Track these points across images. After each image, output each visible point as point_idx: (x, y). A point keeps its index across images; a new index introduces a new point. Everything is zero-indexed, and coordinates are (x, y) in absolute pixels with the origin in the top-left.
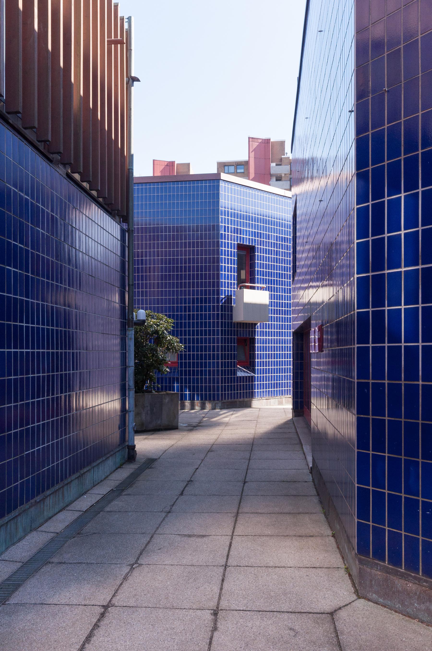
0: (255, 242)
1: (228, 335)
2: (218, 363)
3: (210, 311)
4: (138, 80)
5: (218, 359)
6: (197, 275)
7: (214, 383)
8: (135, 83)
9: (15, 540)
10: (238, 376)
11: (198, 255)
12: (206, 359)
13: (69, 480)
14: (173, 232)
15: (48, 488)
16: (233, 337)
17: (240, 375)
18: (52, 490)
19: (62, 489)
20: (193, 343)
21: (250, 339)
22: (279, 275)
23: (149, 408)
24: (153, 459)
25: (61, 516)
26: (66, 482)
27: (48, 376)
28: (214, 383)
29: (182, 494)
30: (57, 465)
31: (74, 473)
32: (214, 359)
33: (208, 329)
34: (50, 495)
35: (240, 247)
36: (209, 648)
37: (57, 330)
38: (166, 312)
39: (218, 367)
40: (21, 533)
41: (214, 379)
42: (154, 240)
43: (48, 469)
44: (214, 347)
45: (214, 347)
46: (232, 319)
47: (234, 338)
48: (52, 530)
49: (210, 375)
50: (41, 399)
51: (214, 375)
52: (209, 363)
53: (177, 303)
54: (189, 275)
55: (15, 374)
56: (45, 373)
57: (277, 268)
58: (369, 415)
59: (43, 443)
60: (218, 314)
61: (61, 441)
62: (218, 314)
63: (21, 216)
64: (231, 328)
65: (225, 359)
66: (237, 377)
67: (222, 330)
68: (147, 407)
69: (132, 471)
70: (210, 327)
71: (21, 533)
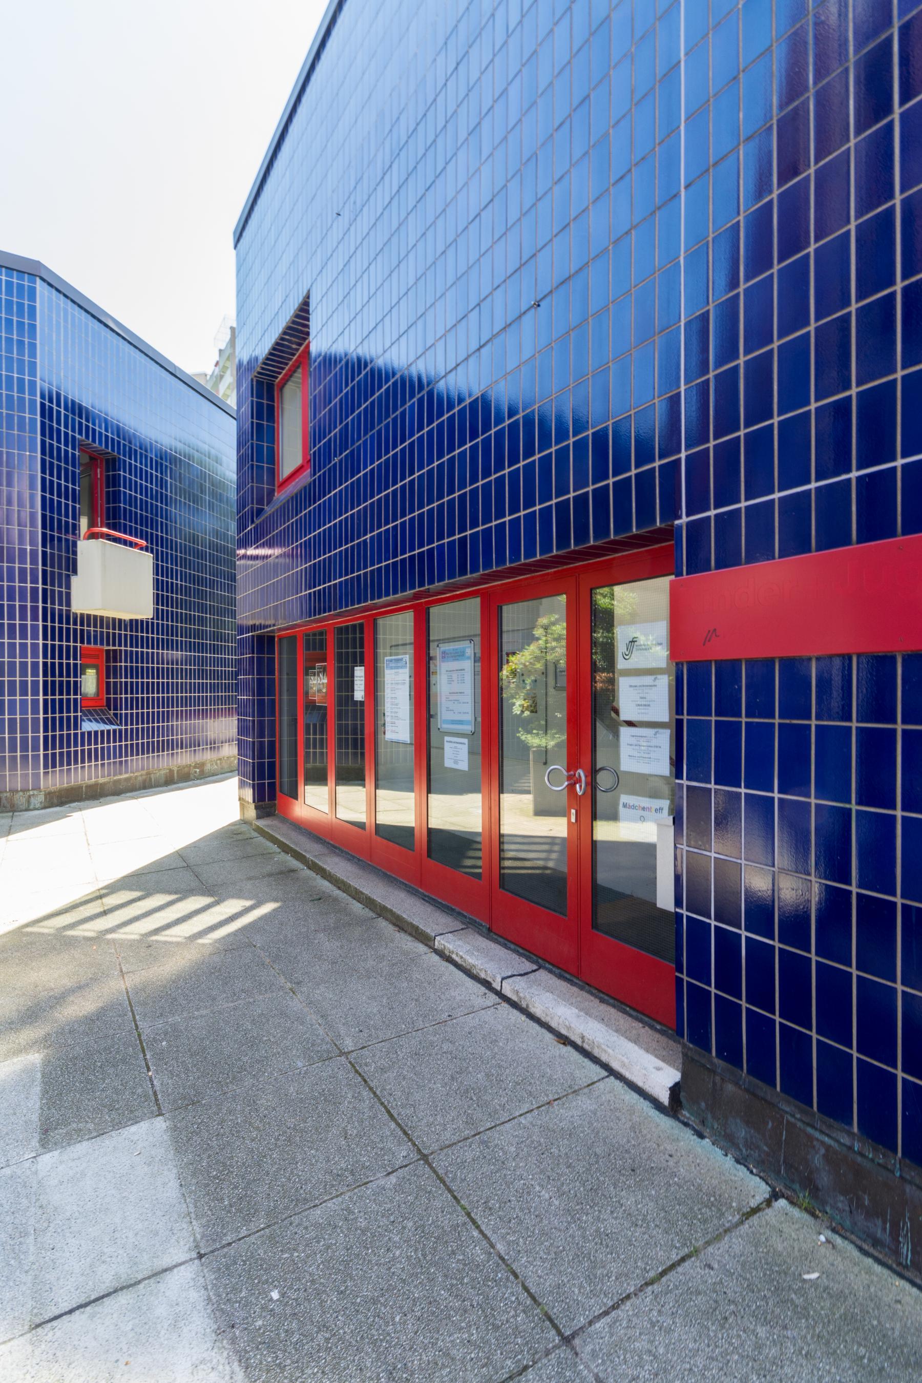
10: (83, 730)
16: (65, 697)
17: (89, 729)
33: (18, 698)
36: (590, 3)
46: (68, 604)
58: (894, 807)
66: (83, 734)
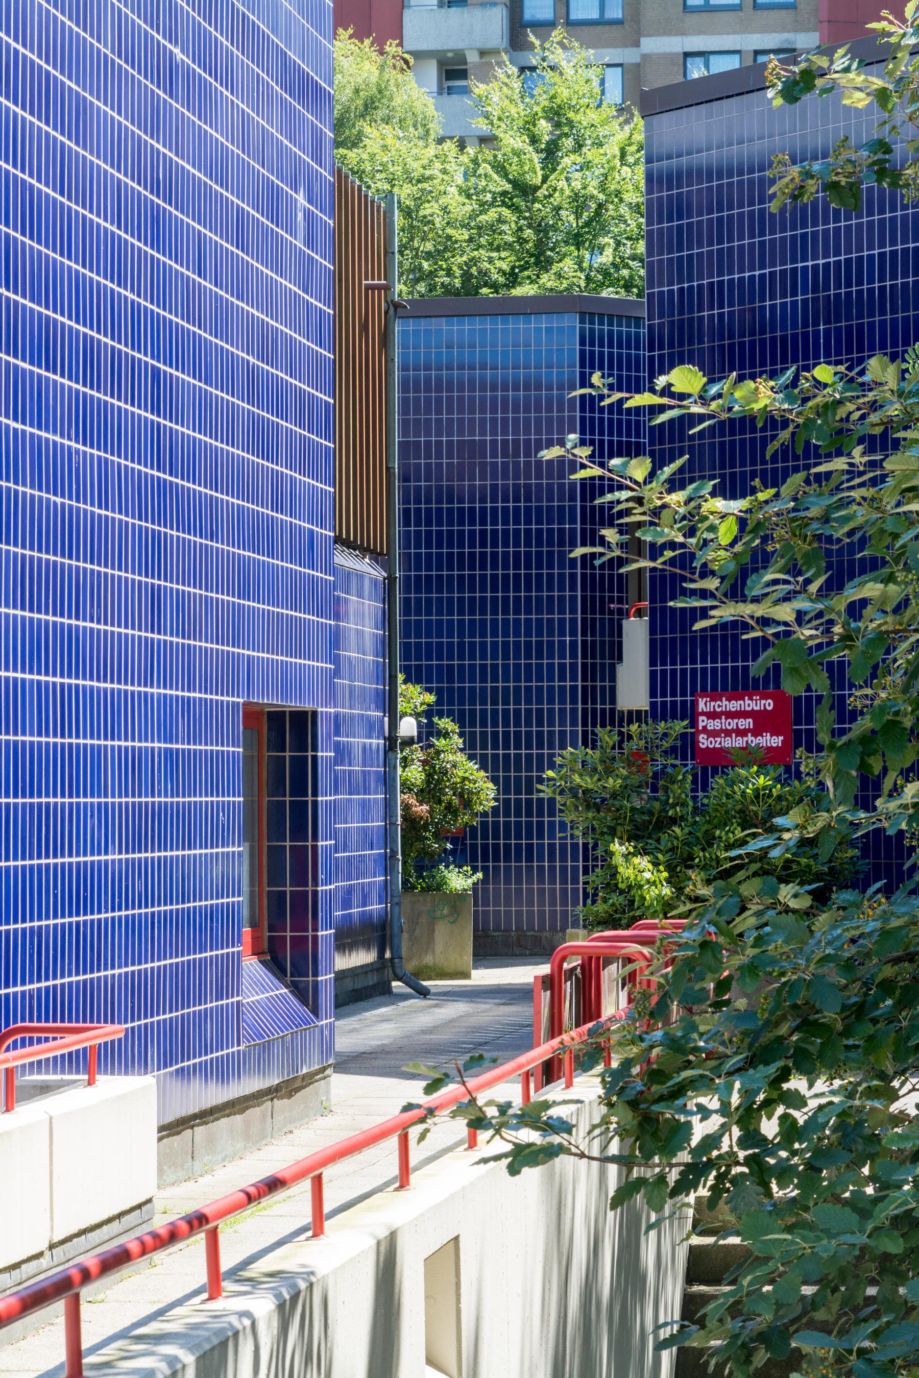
3: (551, 679)
6: (517, 577)
38: (429, 681)
46: (613, 700)
50: (685, 221)
54: (494, 577)
60: (574, 689)
62: (574, 689)
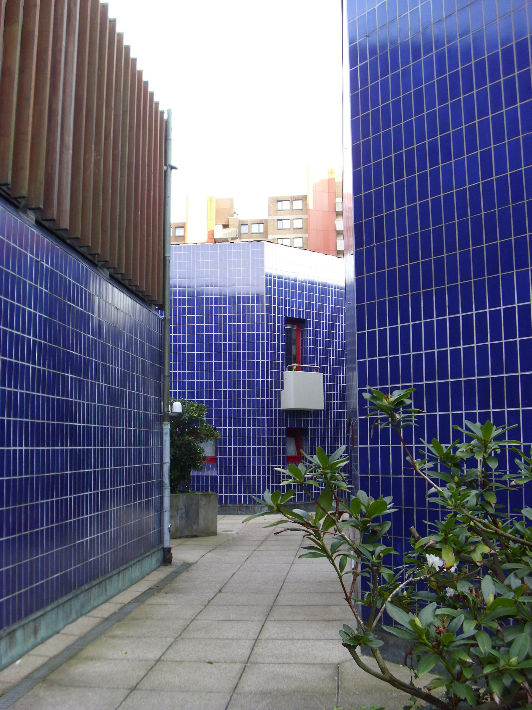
0: (306, 315)
1: (275, 426)
2: (264, 458)
4: (175, 168)
5: (264, 454)
7: (259, 482)
8: (173, 170)
9: (70, 620)
11: (239, 331)
12: (249, 454)
13: (111, 574)
14: (211, 304)
15: (94, 579)
18: (97, 581)
19: (104, 582)
20: (235, 435)
21: (306, 429)
22: (335, 353)
23: (184, 511)
24: (188, 564)
25: (105, 606)
26: (108, 576)
27: (95, 472)
28: (259, 482)
29: (220, 591)
30: (101, 557)
31: (114, 569)
32: (259, 454)
34: (95, 586)
35: (289, 321)
37: (101, 428)
39: (264, 463)
40: (74, 616)
41: (259, 478)
42: (189, 314)
43: (94, 560)
44: (259, 439)
45: (259, 439)
46: (280, 406)
47: (283, 429)
48: (99, 615)
49: (254, 473)
51: (259, 473)
52: (254, 458)
53: (216, 388)
55: (71, 470)
56: (28, 474)
57: (333, 345)
59: (90, 535)
61: (111, 532)
63: (77, 328)
64: (279, 416)
65: (272, 454)
67: (268, 419)
68: (182, 509)
69: (168, 573)
70: (254, 415)
71: (74, 616)
